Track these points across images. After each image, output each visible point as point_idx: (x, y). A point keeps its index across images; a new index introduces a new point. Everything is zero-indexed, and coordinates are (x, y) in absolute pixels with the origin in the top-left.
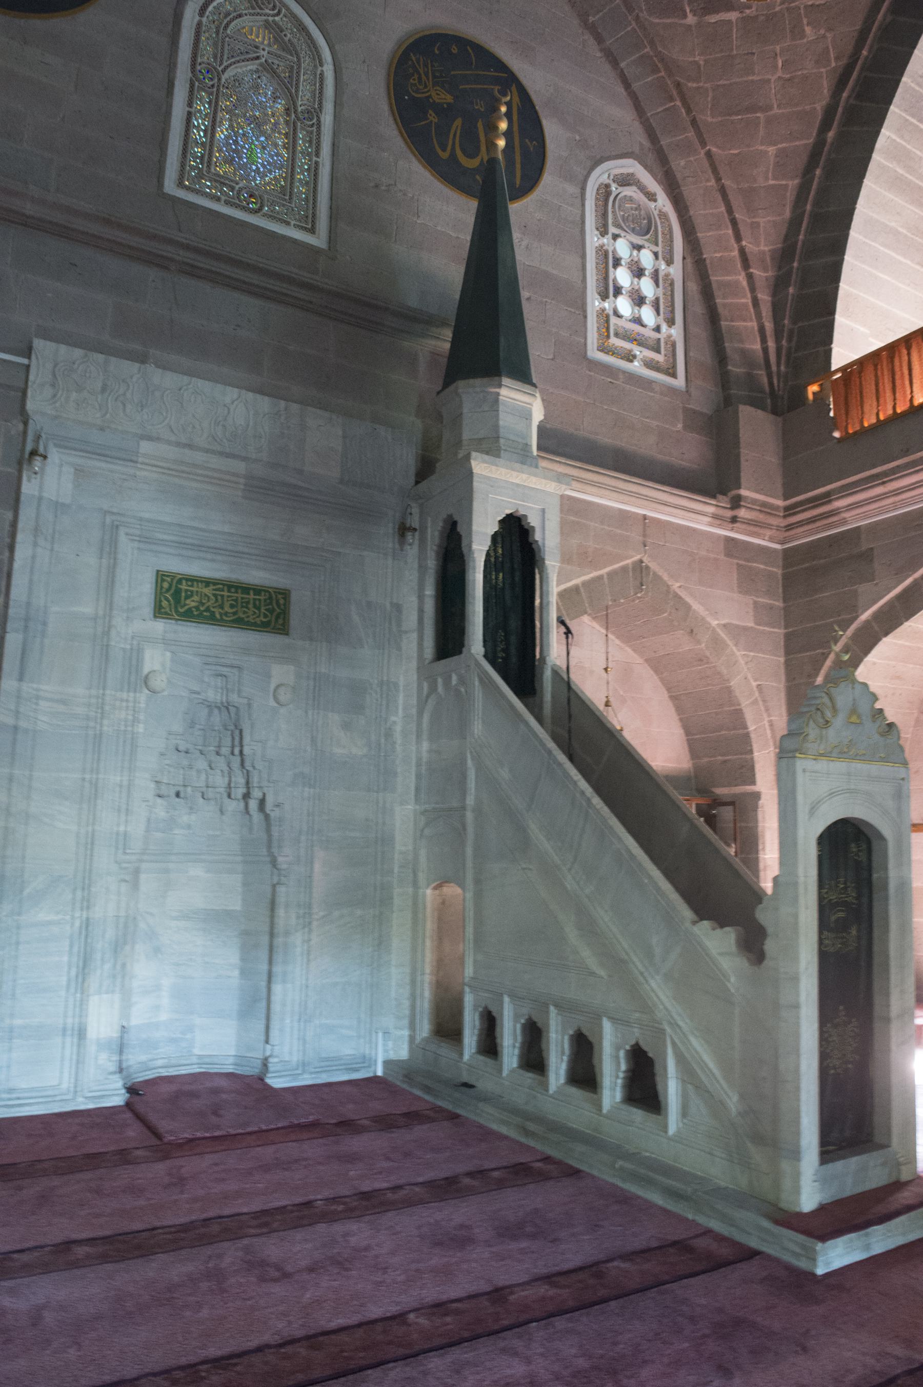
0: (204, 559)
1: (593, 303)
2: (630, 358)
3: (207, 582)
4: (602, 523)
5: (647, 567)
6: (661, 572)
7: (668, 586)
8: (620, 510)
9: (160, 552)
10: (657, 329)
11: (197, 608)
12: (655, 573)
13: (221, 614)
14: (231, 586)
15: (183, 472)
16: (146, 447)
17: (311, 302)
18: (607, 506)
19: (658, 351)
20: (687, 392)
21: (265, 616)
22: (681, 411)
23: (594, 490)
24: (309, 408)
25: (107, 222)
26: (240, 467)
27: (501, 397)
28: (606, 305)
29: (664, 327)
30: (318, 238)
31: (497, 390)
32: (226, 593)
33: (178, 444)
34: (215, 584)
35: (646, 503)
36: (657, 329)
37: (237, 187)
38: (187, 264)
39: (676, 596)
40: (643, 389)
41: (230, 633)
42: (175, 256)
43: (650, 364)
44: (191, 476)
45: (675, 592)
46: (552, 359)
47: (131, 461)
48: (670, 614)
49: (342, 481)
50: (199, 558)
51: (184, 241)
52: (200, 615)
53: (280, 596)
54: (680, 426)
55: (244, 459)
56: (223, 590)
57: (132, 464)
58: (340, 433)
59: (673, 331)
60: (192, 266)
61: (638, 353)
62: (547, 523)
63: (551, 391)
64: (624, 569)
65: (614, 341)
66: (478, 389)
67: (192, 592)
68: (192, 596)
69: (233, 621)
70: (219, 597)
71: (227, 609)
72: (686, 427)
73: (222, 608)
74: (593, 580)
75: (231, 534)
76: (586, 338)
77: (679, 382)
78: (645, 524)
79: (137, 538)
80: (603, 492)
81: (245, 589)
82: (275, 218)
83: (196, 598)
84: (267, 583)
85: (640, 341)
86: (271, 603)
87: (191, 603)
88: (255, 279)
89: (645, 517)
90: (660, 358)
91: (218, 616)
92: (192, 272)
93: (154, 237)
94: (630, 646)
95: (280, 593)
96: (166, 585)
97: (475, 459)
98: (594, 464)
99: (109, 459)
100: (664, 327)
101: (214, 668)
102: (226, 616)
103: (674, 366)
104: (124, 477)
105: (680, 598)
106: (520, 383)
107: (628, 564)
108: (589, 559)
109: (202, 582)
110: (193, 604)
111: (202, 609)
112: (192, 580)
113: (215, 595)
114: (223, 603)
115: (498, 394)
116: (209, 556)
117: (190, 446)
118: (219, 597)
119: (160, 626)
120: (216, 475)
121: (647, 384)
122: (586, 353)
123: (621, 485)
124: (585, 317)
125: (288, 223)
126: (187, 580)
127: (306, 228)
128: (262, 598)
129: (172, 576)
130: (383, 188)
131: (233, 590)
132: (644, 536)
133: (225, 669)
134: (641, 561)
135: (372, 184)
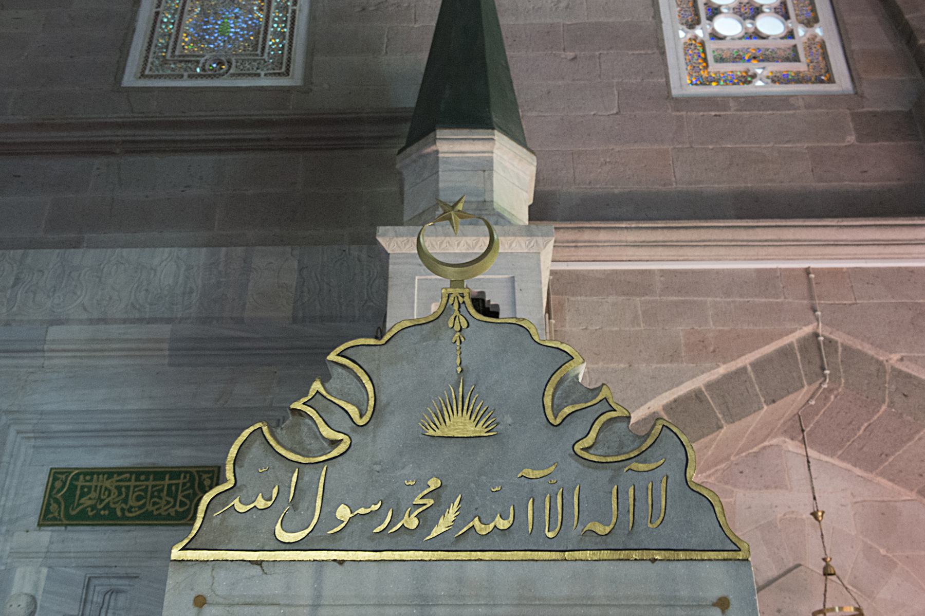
0: (113, 446)
1: (676, 35)
2: (747, 79)
3: (110, 473)
4: (727, 294)
5: (830, 342)
6: (857, 344)
7: (880, 363)
8: (758, 271)
9: (58, 447)
10: (790, 35)
11: (93, 507)
12: (846, 348)
13: (122, 510)
14: (139, 473)
15: (95, 351)
16: (55, 332)
17: (268, 140)
18: (733, 270)
19: (796, 59)
20: (856, 93)
21: (182, 504)
22: (849, 119)
23: (698, 252)
24: (257, 248)
25: (40, 126)
26: (165, 330)
27: (440, 155)
28: (699, 32)
29: (801, 31)
30: (292, 78)
31: (433, 148)
32: (132, 483)
33: (91, 322)
34: (120, 474)
35: (800, 250)
36: (790, 35)
37: (202, 60)
38: (129, 142)
39: (898, 374)
40: (773, 109)
41: (135, 533)
42: (113, 138)
43: (776, 79)
44: (106, 354)
45: (893, 369)
46: (617, 113)
47: (37, 351)
48: (892, 404)
49: (295, 320)
50: (106, 446)
51: (120, 120)
52: (98, 516)
53: (205, 476)
54: (851, 139)
55: (169, 321)
56: (130, 480)
57: (38, 354)
58: (296, 264)
59: (818, 31)
60: (134, 142)
61: (759, 71)
62: (518, 295)
63: (617, 149)
64: (786, 352)
65: (715, 68)
66: (414, 157)
67: (90, 488)
68: (89, 492)
69: (138, 518)
70: (123, 489)
71: (132, 502)
72: (860, 138)
73: (126, 503)
74: (728, 377)
75: (149, 411)
76: (667, 76)
77: (843, 83)
78: (809, 280)
79: (32, 435)
80: (715, 251)
81: (159, 474)
82: (244, 75)
83: (93, 495)
84: (186, 462)
85: (765, 57)
86: (192, 487)
87: (86, 502)
88: (202, 134)
89: (807, 271)
90: (801, 67)
91: (119, 513)
92: (134, 148)
93: (90, 126)
94: (882, 474)
95: (205, 472)
96: (58, 484)
97: (384, 235)
98: (706, 218)
99: (14, 355)
100: (801, 31)
101: (106, 581)
102: (130, 511)
103: (828, 70)
104: (31, 370)
105: (909, 376)
106: (465, 131)
107: (791, 345)
108: (712, 349)
109: (104, 474)
110: (89, 503)
111: (100, 507)
112: (91, 473)
113: (117, 487)
114: (127, 496)
115: (437, 152)
116: (119, 441)
117: (104, 321)
118: (123, 489)
119: (46, 535)
120: (134, 346)
121: (784, 101)
122: (669, 92)
123: (743, 235)
124: (663, 53)
125: (259, 75)
126: (86, 474)
127: (279, 74)
128: (181, 481)
129: (66, 472)
130: (373, 8)
131: (143, 477)
132: (812, 297)
133: (121, 582)
134: (816, 335)
135: (359, 9)
